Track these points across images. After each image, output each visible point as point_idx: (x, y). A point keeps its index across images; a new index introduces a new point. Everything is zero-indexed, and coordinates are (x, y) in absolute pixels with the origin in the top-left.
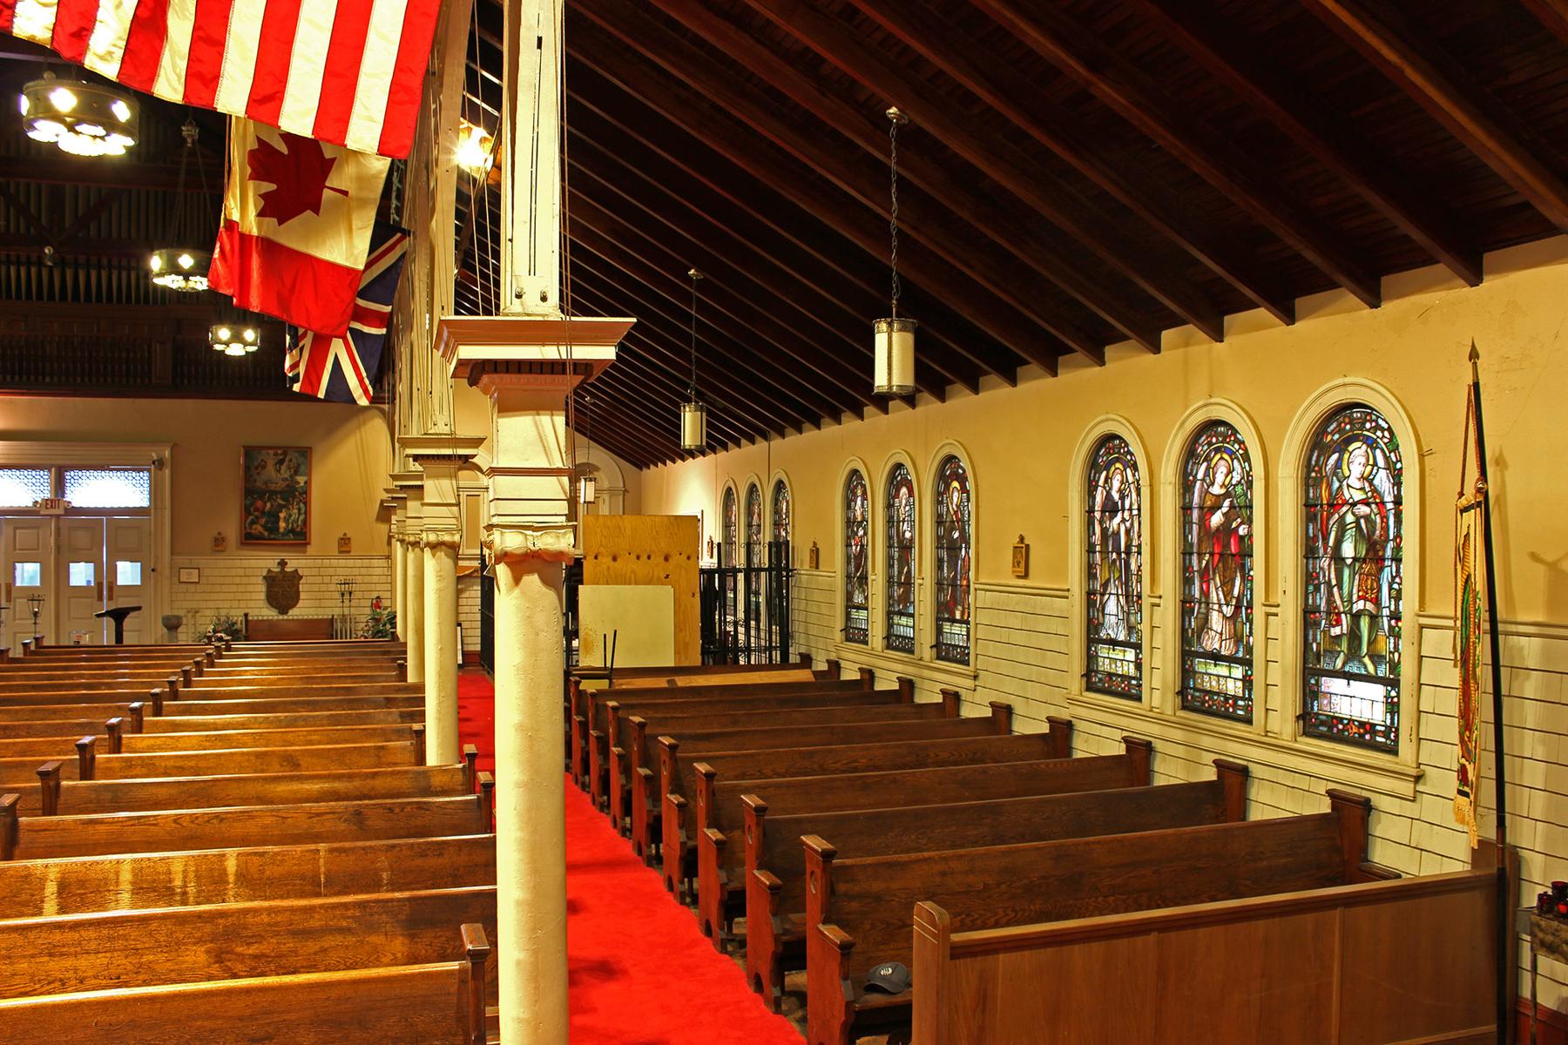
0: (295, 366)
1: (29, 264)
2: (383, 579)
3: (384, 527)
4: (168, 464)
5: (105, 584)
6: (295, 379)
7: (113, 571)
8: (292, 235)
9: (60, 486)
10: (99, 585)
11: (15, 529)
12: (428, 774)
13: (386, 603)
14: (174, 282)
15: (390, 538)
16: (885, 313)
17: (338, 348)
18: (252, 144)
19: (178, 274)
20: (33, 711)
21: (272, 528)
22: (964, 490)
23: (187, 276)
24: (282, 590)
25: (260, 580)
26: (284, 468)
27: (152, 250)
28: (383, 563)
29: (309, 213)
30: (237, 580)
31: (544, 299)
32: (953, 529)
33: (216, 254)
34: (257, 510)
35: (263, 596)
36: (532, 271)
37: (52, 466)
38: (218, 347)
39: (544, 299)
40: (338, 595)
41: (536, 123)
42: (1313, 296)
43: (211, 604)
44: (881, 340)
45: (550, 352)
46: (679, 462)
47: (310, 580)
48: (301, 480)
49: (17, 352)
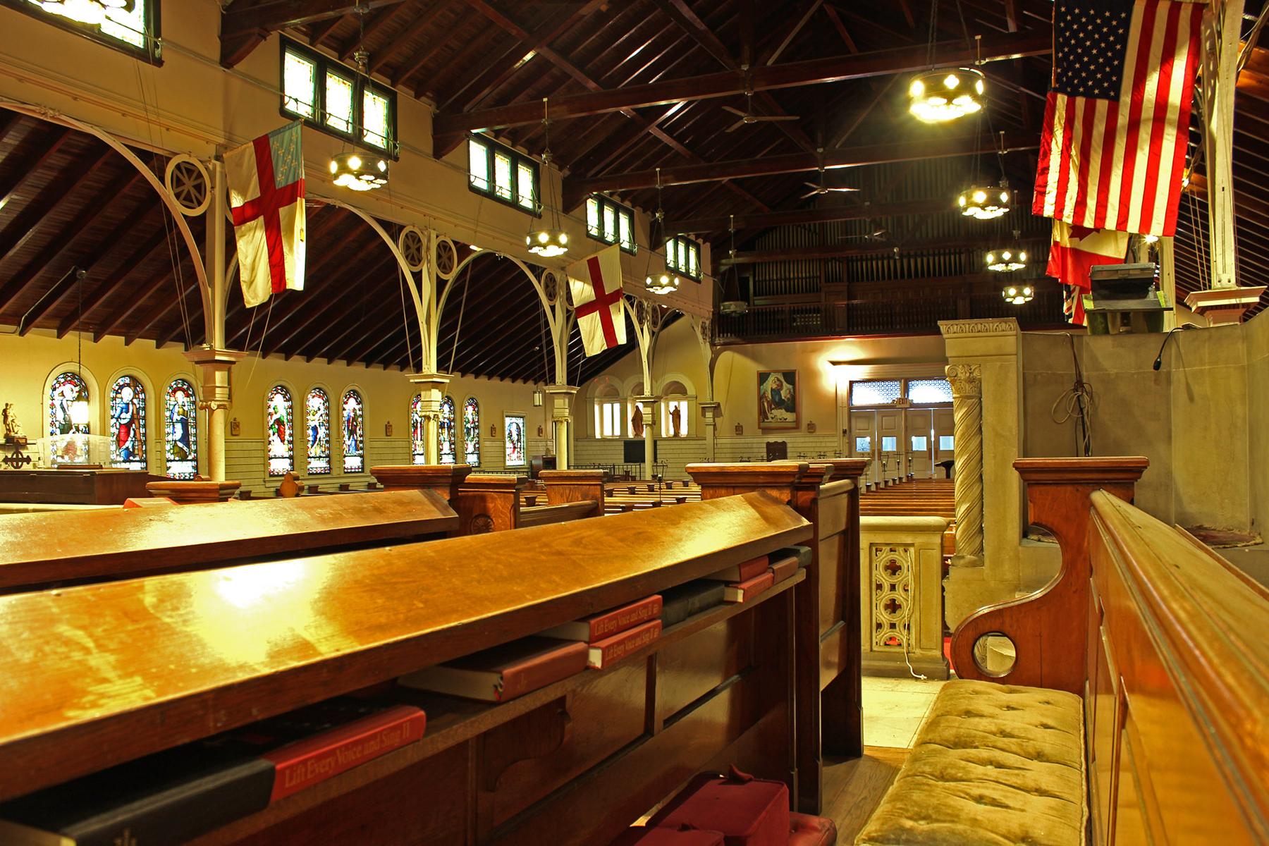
0: (1069, 309)
1: (883, 259)
5: (933, 449)
6: (1070, 316)
7: (937, 442)
9: (906, 390)
10: (929, 449)
14: (1000, 268)
19: (1002, 263)
23: (1007, 263)
27: (988, 250)
31: (1229, 281)
33: (1050, 259)
36: (1224, 271)
37: (902, 379)
38: (1008, 300)
39: (1229, 281)
41: (1223, 217)
45: (1233, 301)
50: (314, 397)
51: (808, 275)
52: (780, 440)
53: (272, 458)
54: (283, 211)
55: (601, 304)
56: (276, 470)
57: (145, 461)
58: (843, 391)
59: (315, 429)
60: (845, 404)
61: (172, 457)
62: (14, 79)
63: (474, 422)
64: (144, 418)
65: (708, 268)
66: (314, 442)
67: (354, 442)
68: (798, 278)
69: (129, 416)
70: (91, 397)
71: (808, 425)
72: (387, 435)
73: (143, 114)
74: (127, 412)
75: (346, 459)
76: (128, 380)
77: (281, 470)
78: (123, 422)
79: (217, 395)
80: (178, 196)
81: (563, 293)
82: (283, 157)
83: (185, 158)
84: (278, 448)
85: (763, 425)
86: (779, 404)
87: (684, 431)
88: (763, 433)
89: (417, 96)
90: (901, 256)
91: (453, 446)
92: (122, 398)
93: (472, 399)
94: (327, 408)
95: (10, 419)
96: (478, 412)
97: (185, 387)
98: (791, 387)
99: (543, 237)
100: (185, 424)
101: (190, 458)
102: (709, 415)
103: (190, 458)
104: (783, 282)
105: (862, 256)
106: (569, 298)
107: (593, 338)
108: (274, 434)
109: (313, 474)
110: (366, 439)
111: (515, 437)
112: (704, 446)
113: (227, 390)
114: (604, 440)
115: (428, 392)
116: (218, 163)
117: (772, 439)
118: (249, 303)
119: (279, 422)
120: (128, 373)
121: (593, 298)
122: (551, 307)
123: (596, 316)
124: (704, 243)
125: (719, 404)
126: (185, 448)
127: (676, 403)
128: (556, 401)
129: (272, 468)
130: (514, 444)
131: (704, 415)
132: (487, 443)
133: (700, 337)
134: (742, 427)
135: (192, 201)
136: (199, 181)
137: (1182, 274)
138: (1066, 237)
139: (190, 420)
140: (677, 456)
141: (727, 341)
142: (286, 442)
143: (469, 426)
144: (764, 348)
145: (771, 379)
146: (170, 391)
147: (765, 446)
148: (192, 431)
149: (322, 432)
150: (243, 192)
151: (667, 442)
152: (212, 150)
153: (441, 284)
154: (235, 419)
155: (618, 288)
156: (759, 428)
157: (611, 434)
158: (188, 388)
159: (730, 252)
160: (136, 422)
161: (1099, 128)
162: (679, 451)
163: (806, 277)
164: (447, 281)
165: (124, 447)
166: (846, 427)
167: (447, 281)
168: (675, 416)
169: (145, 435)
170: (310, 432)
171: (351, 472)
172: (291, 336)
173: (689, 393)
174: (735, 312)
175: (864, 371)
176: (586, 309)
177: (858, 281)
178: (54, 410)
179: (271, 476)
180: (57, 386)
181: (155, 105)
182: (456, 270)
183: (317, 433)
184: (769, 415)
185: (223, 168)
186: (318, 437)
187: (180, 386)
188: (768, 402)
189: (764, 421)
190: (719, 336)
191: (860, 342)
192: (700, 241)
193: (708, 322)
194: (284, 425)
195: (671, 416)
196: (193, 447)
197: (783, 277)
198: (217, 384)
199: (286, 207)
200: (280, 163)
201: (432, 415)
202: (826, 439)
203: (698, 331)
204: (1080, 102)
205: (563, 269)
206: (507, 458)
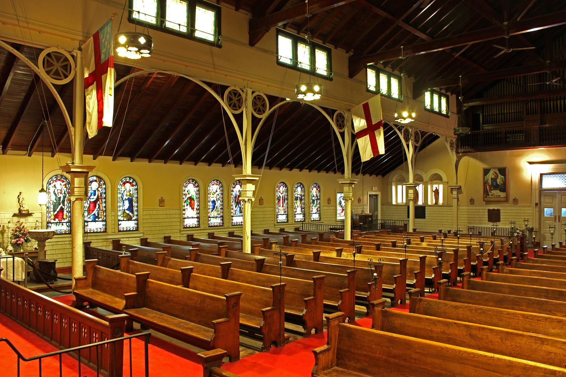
2: (257, 223)
11: (562, 196)
20: (365, 256)
42: (456, 100)
49: (562, 131)
50: (213, 184)
51: (515, 111)
52: (496, 208)
53: (186, 218)
55: (370, 130)
56: (188, 225)
57: (105, 221)
58: (536, 179)
59: (214, 202)
60: (537, 187)
61: (122, 219)
63: (317, 196)
64: (105, 198)
65: (455, 109)
66: (213, 209)
67: (239, 209)
68: (509, 113)
69: (96, 197)
71: (514, 199)
72: (260, 204)
73: (16, 22)
74: (95, 195)
75: (234, 218)
76: (95, 178)
77: (191, 224)
78: (92, 200)
79: (75, 193)
80: (48, 73)
81: (349, 124)
83: (55, 50)
84: (190, 212)
85: (486, 199)
86: (496, 187)
87: (441, 201)
88: (486, 204)
89: (237, 10)
91: (303, 210)
92: (91, 188)
93: (316, 184)
94: (222, 190)
95: (21, 200)
96: (320, 191)
97: (131, 181)
98: (503, 177)
99: (303, 88)
100: (131, 201)
101: (133, 219)
103: (133, 219)
104: (500, 116)
105: (550, 98)
106: (353, 127)
107: (366, 151)
108: (187, 205)
109: (212, 226)
112: (451, 210)
113: (83, 189)
114: (397, 205)
115: (245, 186)
116: (79, 52)
119: (191, 199)
120: (95, 174)
121: (366, 127)
122: (340, 133)
124: (451, 95)
125: (460, 187)
126: (131, 214)
127: (437, 186)
128: (344, 188)
129: (185, 224)
131: (452, 193)
132: (325, 208)
133: (449, 148)
134: (474, 200)
135: (234, 93)
136: (65, 63)
139: (134, 199)
140: (436, 215)
141: (465, 150)
142: (195, 209)
143: (314, 198)
144: (487, 154)
145: (491, 172)
146: (122, 183)
147: (487, 211)
148: (135, 204)
149: (218, 204)
151: (431, 208)
152: (77, 44)
153: (255, 121)
154: (162, 198)
155: (379, 121)
156: (484, 201)
157: (401, 202)
158: (133, 182)
159: (460, 98)
160: (100, 200)
162: (437, 213)
163: (514, 113)
164: (261, 119)
165: (92, 214)
166: (537, 201)
167: (261, 119)
168: (436, 193)
169: (105, 207)
170: (211, 204)
171: (237, 225)
172: (279, 152)
173: (444, 180)
174: (462, 133)
175: (548, 168)
176: (362, 133)
177: (547, 113)
178: (50, 195)
179: (184, 228)
180: (52, 182)
181: (25, 17)
182: (268, 112)
183: (215, 204)
184: (490, 194)
185: (82, 54)
186: (216, 206)
187: (128, 180)
188: (489, 186)
189: (486, 197)
190: (461, 148)
191: (556, 150)
192: (449, 94)
193: (454, 140)
194: (194, 200)
195: (434, 193)
196: (136, 213)
197: (500, 113)
201: (246, 199)
202: (524, 209)
203: (448, 146)
205: (349, 110)
206: (338, 215)
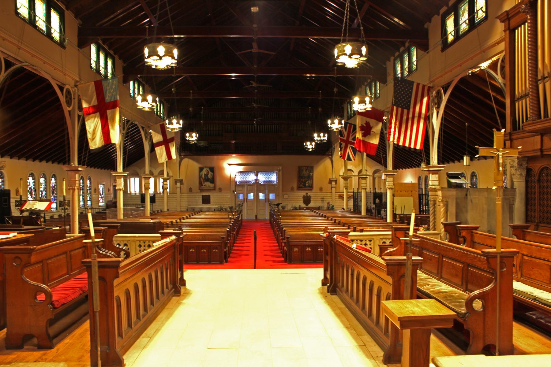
2: (330, 197)
3: (331, 185)
4: (281, 171)
5: (267, 199)
8: (367, 139)
9: (257, 175)
10: (266, 199)
12: (388, 223)
13: (331, 203)
15: (332, 188)
16: (465, 154)
17: (348, 150)
18: (360, 125)
21: (305, 186)
22: (476, 178)
24: (307, 200)
25: (302, 198)
26: (307, 171)
27: (315, 133)
28: (330, 194)
29: (369, 136)
30: (297, 198)
32: (474, 185)
34: (301, 181)
35: (302, 201)
36: (435, 160)
40: (321, 201)
43: (291, 203)
44: (465, 158)
45: (438, 169)
46: (404, 169)
47: (313, 197)
48: (311, 174)
52: (207, 194)
54: (109, 112)
59: (42, 191)
62: (30, 55)
70: (5, 184)
71: (219, 188)
79: (77, 184)
82: (109, 90)
86: (207, 180)
90: (257, 124)
94: (46, 182)
98: (212, 173)
102: (178, 184)
110: (58, 196)
111: (102, 194)
115: (120, 179)
116: (76, 88)
117: (204, 194)
118: (92, 147)
123: (163, 147)
125: (182, 180)
130: (101, 196)
131: (176, 184)
132: (94, 196)
137: (398, 151)
138: (361, 136)
144: (202, 158)
145: (205, 170)
150: (88, 102)
161: (405, 117)
166: (234, 190)
175: (241, 168)
176: (159, 144)
184: (203, 185)
188: (203, 179)
198: (77, 180)
199: (110, 110)
200: (108, 92)
204: (400, 109)
